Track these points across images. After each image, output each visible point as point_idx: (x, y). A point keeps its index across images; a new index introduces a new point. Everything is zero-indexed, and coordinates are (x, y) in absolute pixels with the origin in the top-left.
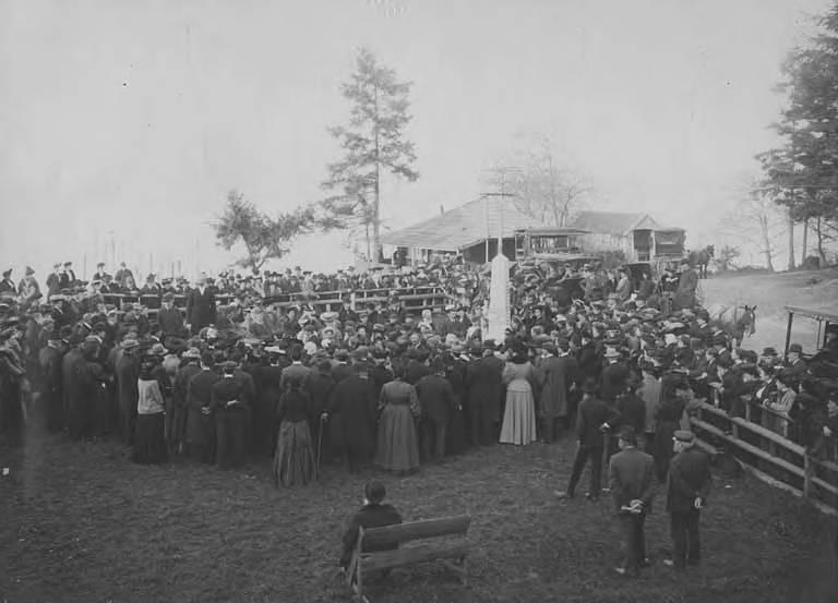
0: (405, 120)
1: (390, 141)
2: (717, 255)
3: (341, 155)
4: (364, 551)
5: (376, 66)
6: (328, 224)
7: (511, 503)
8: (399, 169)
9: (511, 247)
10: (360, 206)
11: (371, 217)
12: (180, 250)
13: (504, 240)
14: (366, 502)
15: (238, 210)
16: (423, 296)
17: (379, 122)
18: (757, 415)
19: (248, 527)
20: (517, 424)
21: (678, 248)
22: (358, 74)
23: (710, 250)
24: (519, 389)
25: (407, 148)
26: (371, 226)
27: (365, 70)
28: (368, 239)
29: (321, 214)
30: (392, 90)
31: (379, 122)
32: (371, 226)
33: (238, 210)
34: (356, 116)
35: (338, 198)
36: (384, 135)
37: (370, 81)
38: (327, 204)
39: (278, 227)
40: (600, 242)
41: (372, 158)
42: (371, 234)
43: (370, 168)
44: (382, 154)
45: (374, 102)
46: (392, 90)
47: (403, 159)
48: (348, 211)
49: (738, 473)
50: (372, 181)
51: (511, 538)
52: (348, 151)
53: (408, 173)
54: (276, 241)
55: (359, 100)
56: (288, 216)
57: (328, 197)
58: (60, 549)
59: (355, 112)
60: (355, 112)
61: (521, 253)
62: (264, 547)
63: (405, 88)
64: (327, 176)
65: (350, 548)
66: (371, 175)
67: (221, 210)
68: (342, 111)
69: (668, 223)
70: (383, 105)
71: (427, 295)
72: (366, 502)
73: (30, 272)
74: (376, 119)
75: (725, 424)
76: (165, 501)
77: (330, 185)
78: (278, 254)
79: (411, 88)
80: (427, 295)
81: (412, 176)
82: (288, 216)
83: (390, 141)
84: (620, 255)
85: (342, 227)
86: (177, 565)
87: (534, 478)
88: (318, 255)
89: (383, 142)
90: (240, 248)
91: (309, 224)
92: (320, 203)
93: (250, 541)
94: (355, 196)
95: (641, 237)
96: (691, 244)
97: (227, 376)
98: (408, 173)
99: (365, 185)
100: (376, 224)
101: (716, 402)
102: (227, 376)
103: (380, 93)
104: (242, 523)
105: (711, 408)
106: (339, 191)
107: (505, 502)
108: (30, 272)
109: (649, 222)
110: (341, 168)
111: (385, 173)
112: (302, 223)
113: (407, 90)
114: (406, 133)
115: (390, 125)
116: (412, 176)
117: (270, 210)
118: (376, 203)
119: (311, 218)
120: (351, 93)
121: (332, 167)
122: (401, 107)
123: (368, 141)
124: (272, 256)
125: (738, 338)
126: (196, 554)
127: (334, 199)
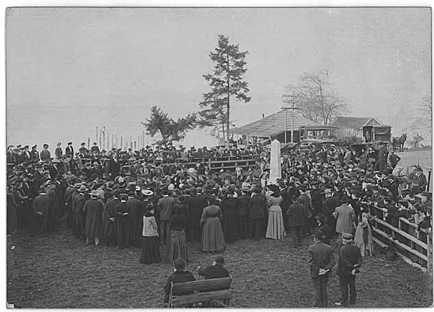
0: (244, 71)
1: (236, 82)
2: (410, 138)
3: (210, 90)
4: (174, 295)
5: (228, 45)
6: (203, 124)
7: (267, 271)
8: (241, 96)
9: (280, 137)
10: (220, 115)
11: (225, 120)
12: (132, 136)
13: (294, 131)
14: (175, 270)
15: (157, 116)
16: (246, 160)
17: (230, 73)
18: (406, 228)
19: (125, 279)
20: (275, 226)
21: (388, 135)
22: (219, 48)
23: (405, 136)
24: (276, 210)
25: (244, 85)
26: (225, 125)
27: (221, 45)
28: (224, 132)
29: (199, 118)
30: (237, 56)
31: (230, 73)
32: (225, 125)
33: (157, 116)
34: (218, 69)
35: (208, 110)
36: (232, 79)
37: (224, 52)
38: (203, 114)
39: (178, 125)
40: (348, 132)
41: (226, 90)
42: (225, 129)
43: (225, 95)
44: (231, 88)
45: (227, 62)
46: (237, 56)
47: (242, 91)
48: (214, 117)
49: (395, 257)
50: (226, 102)
51: (261, 289)
52: (214, 87)
53: (244, 97)
54: (176, 132)
55: (219, 62)
56: (183, 119)
57: (203, 110)
58: (27, 289)
59: (217, 68)
60: (217, 68)
61: (302, 139)
62: (131, 290)
63: (243, 55)
64: (203, 100)
65: (168, 294)
66: (225, 99)
67: (148, 116)
68: (211, 67)
69: (385, 123)
70: (231, 63)
71: (249, 160)
72: (175, 270)
73: (46, 146)
74: (228, 71)
75: (389, 231)
76: (87, 265)
77: (205, 104)
78: (178, 139)
79: (246, 55)
80: (249, 160)
81: (247, 100)
82: (183, 119)
83: (236, 82)
84: (354, 139)
85: (210, 125)
86: (84, 298)
87: (282, 258)
88: (196, 139)
89: (231, 82)
90: (159, 136)
91: (194, 123)
92: (199, 113)
93: (124, 287)
94: (215, 109)
95: (367, 129)
96: (395, 134)
97: (122, 201)
98: (244, 97)
99: (223, 104)
100: (228, 123)
101: (384, 219)
102: (122, 201)
103: (230, 58)
104: (122, 277)
105: (382, 222)
106: (209, 107)
107: (263, 270)
108: (46, 146)
109: (374, 122)
110: (211, 95)
111: (233, 98)
112: (189, 123)
113: (244, 56)
114: (244, 78)
115: (234, 74)
116: (247, 100)
117: (174, 116)
118: (228, 113)
119: (194, 121)
120: (214, 58)
121: (206, 95)
122: (241, 64)
123: (224, 82)
124: (174, 140)
125: (409, 184)
126: (95, 293)
127: (206, 111)
